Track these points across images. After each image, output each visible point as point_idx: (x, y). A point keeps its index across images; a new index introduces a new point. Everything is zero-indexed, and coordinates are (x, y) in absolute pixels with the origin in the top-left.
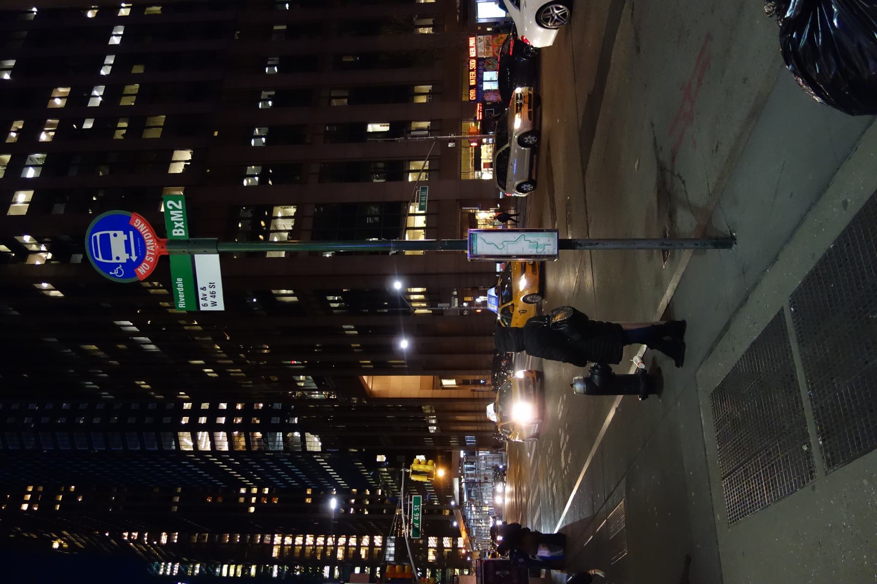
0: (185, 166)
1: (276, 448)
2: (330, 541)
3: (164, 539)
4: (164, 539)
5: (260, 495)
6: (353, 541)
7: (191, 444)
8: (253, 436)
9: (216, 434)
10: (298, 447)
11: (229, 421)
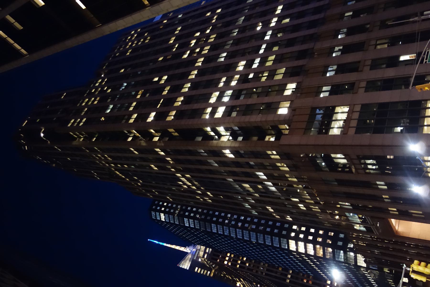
0: (293, 91)
1: (340, 260)
8: (327, 250)
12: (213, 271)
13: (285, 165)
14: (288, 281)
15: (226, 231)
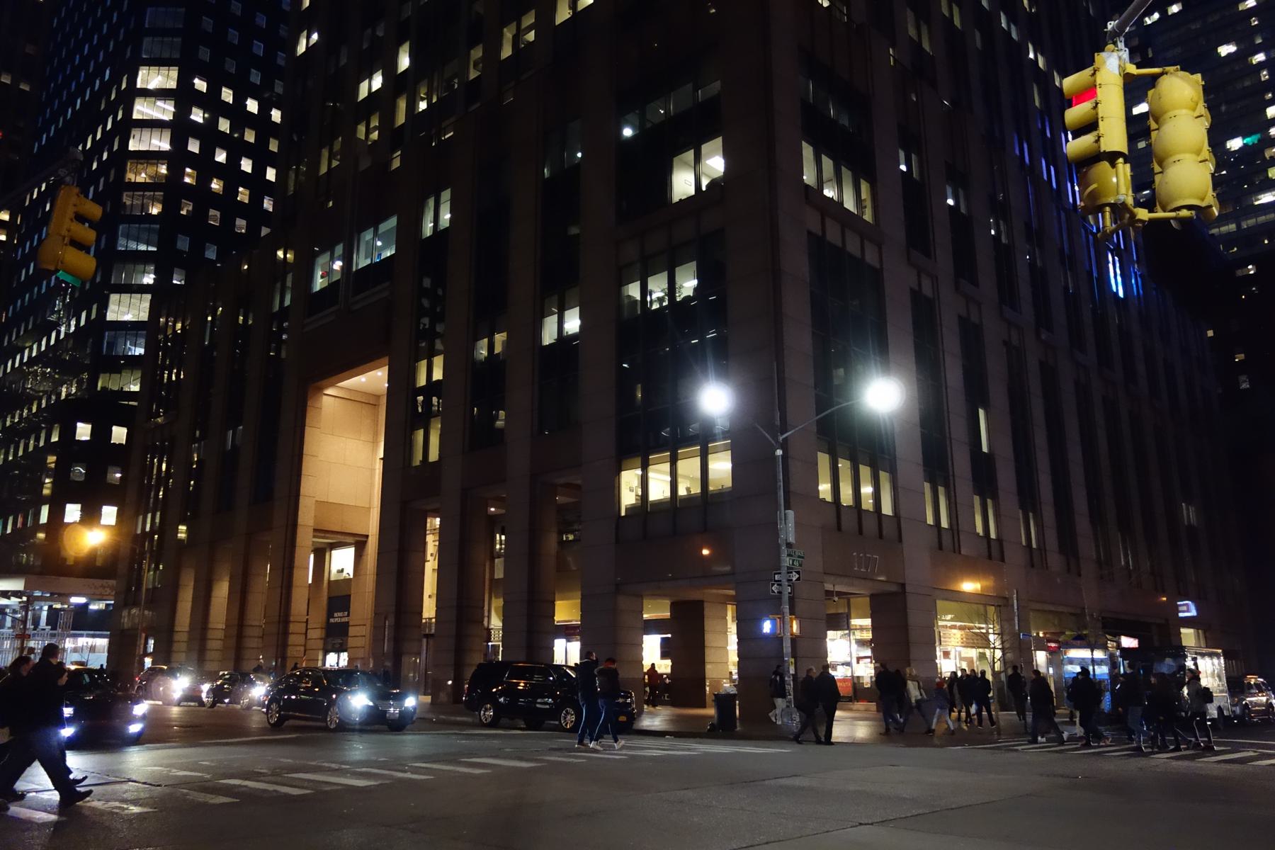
7: (151, 86)
9: (167, 135)
11: (192, 160)
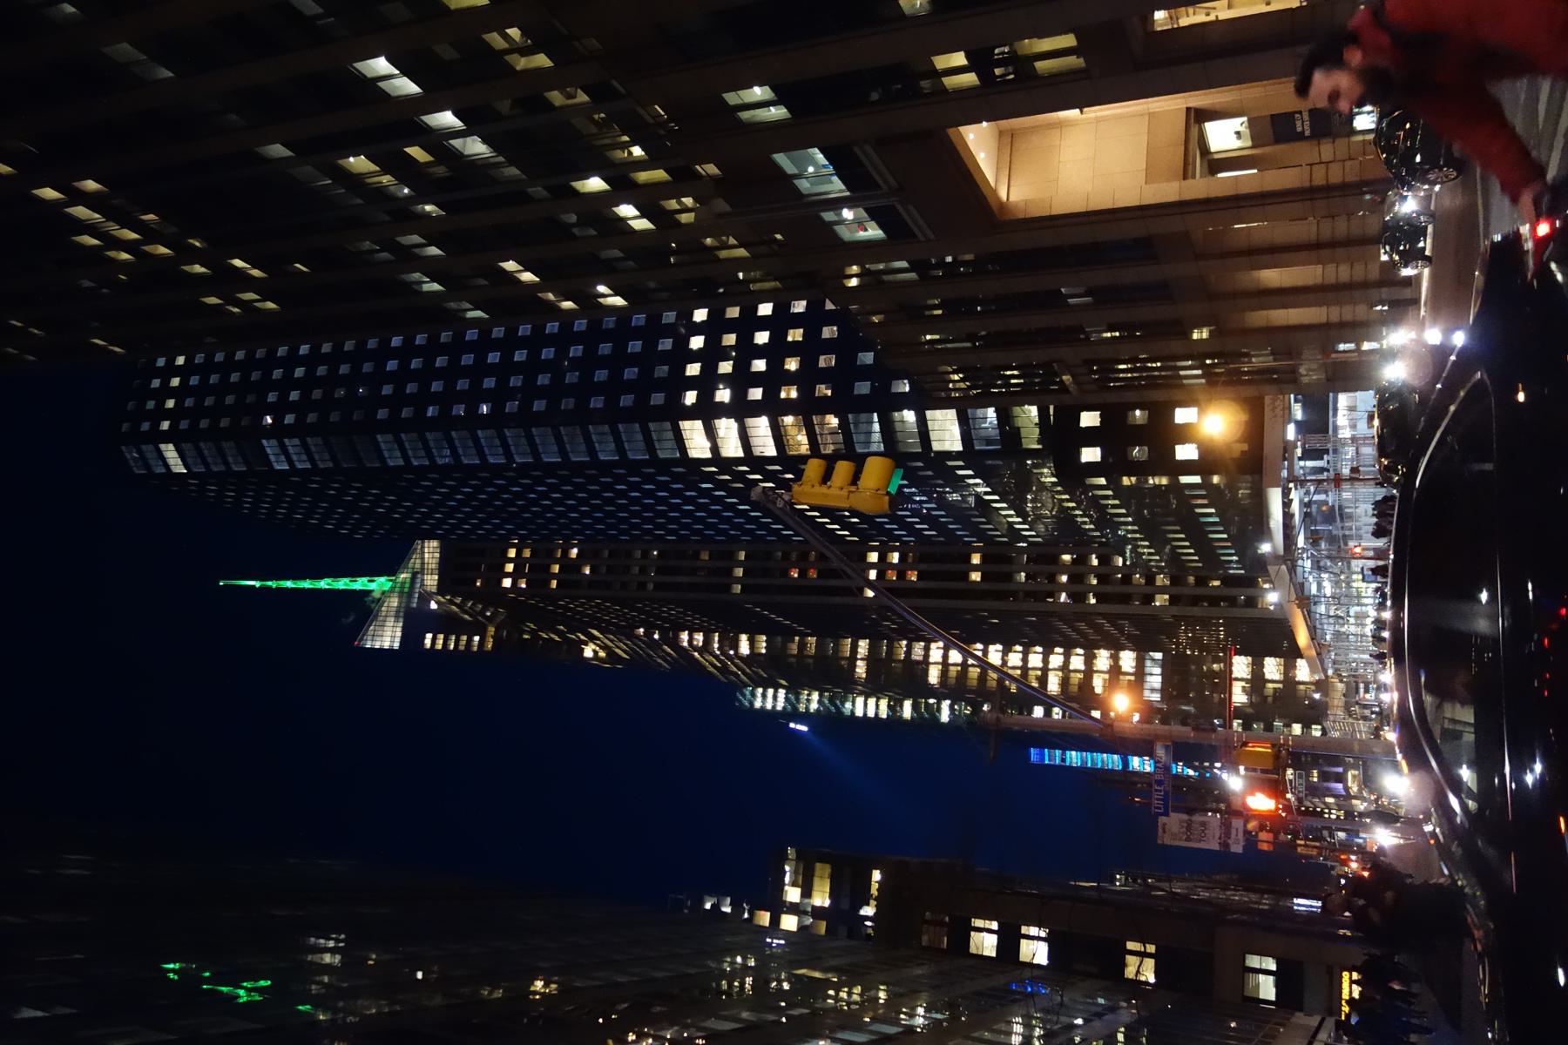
2: (1035, 660)
3: (744, 648)
4: (744, 648)
5: (883, 565)
6: (1077, 662)
8: (822, 424)
10: (913, 444)
12: (491, 630)
13: (732, 241)
14: (737, 588)
15: (441, 448)
